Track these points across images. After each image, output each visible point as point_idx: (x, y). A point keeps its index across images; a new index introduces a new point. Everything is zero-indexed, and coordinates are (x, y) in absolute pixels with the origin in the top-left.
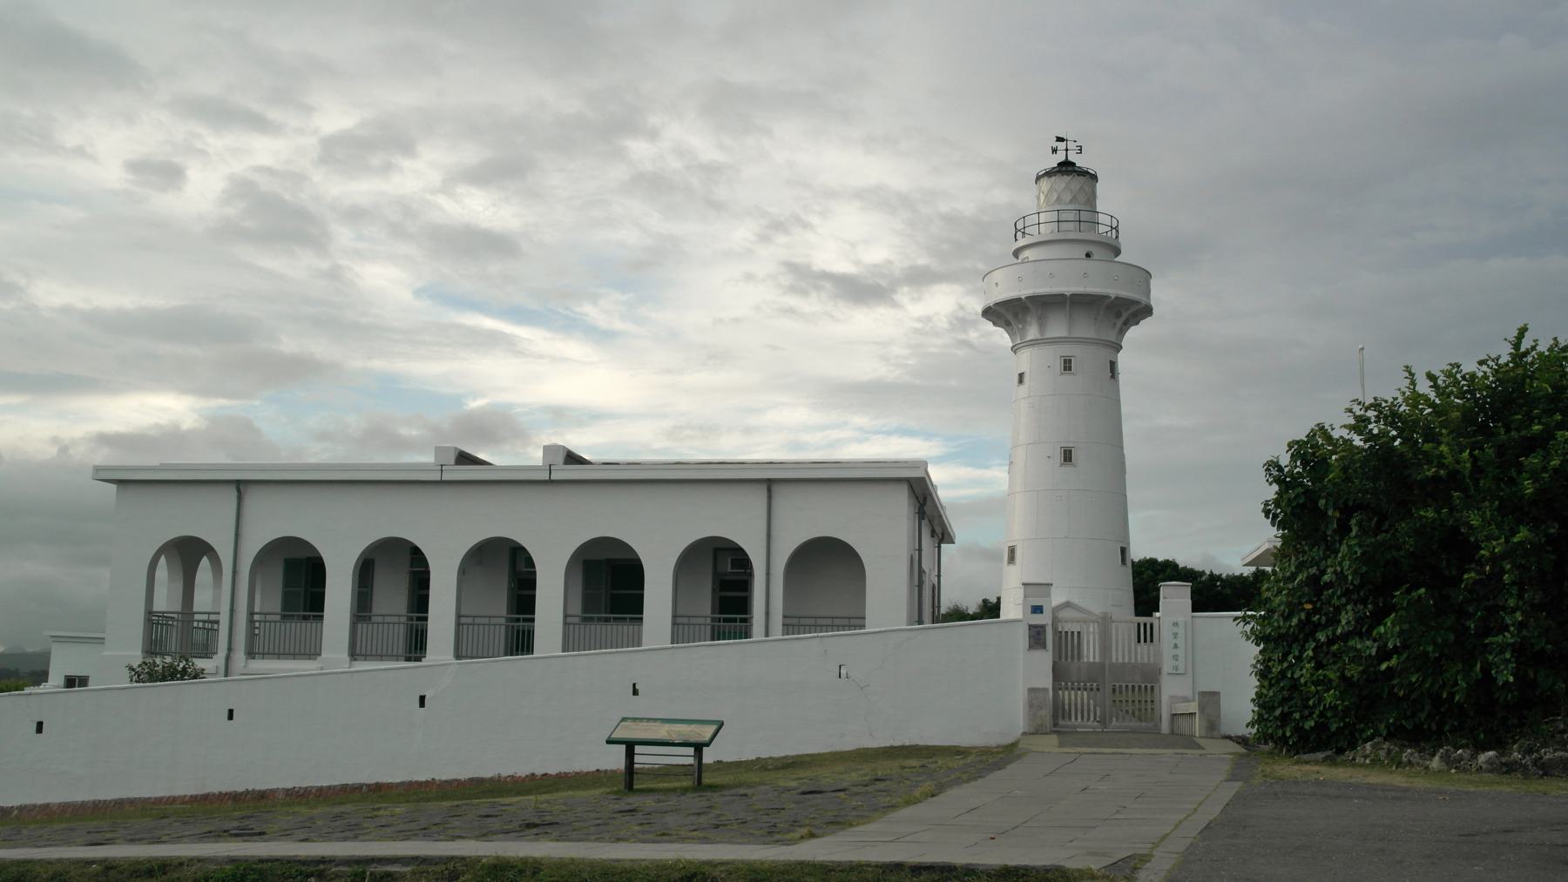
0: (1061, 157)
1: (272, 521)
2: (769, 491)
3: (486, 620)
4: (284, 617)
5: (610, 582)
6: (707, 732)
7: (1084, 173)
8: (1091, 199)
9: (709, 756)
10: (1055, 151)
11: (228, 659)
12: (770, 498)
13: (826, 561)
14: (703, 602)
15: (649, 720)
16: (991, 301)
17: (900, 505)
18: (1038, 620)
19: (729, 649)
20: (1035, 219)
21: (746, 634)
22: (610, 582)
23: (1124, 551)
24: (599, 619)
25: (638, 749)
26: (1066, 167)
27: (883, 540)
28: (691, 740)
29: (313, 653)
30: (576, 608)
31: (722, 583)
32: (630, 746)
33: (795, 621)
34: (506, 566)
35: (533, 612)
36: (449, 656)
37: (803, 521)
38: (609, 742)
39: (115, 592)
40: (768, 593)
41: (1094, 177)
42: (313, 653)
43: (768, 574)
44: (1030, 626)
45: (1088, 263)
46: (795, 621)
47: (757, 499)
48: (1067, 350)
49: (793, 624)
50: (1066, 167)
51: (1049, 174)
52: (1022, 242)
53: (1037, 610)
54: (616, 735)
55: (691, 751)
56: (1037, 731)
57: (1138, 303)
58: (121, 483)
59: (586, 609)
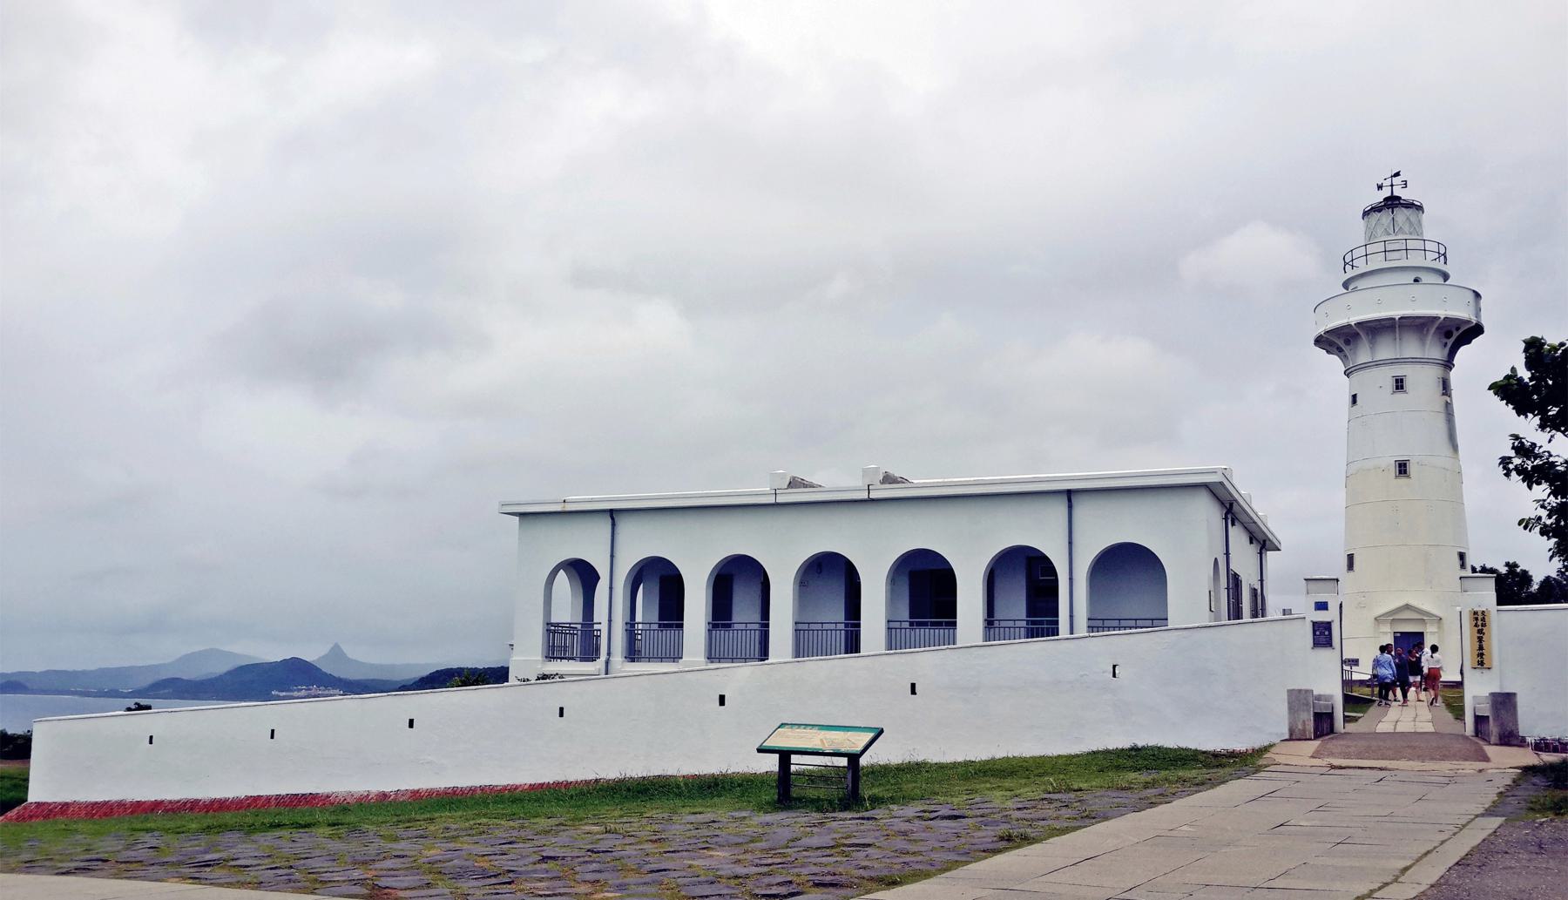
0: (1386, 193)
1: (638, 545)
2: (1070, 501)
3: (1011, 624)
4: (911, 624)
5: (927, 589)
6: (859, 740)
7: (1410, 205)
8: (1416, 229)
9: (863, 761)
10: (1380, 187)
11: (607, 662)
12: (1070, 507)
13: (1127, 566)
14: (1015, 606)
15: (799, 725)
16: (1321, 330)
17: (1206, 512)
18: (1322, 616)
19: (1040, 646)
20: (1362, 251)
21: (1054, 632)
22: (927, 589)
23: (1462, 556)
24: (933, 624)
25: (794, 758)
26: (1392, 202)
27: (1187, 547)
28: (843, 750)
29: (676, 657)
30: (904, 613)
31: (1029, 584)
32: (785, 756)
33: (1100, 623)
34: (831, 573)
35: (954, 616)
36: (702, 658)
37: (1102, 530)
38: (759, 751)
39: (514, 602)
40: (1074, 597)
41: (1420, 208)
42: (676, 657)
43: (1071, 579)
44: (1314, 624)
45: (1417, 287)
46: (1100, 623)
47: (1059, 509)
48: (1399, 371)
49: (1098, 624)
50: (1392, 202)
51: (1376, 209)
52: (1351, 273)
53: (1322, 606)
54: (769, 744)
55: (843, 762)
56: (1294, 736)
57: (1469, 322)
58: (522, 515)
59: (913, 613)
